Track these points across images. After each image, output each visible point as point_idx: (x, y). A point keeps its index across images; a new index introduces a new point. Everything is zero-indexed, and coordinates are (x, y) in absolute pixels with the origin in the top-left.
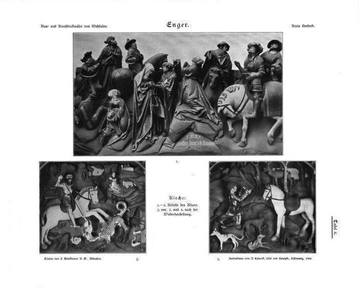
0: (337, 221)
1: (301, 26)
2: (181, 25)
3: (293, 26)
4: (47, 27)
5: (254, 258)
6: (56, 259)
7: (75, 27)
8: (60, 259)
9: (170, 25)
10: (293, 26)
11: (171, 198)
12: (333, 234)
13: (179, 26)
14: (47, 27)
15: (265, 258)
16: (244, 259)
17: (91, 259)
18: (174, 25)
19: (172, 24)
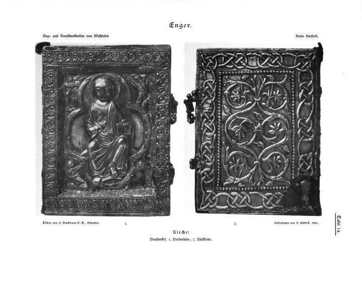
0: (340, 217)
1: (305, 36)
3: (275, 223)
4: (49, 36)
5: (62, 222)
6: (57, 36)
7: (77, 36)
8: (58, 223)
11: (174, 232)
12: (337, 232)
13: (181, 27)
14: (49, 36)
15: (311, 222)
16: (85, 36)
17: (88, 223)
18: (177, 25)
19: (174, 24)
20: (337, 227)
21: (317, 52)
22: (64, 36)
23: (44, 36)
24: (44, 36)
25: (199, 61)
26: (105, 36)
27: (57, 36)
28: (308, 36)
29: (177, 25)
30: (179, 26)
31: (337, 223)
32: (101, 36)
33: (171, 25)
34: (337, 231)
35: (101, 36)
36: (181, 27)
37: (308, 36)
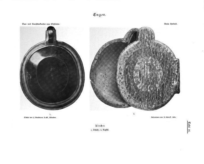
0: (190, 123)
1: (170, 24)
2: (101, 15)
3: (152, 117)
4: (25, 24)
6: (30, 24)
9: (95, 15)
10: (176, 24)
11: (96, 126)
12: (188, 131)
13: (100, 16)
14: (25, 24)
16: (46, 24)
18: (97, 15)
20: (189, 128)
21: (134, 33)
22: (34, 24)
23: (23, 24)
24: (23, 24)
25: (21, 30)
26: (57, 24)
27: (30, 24)
28: (171, 24)
29: (97, 15)
30: (99, 15)
31: (188, 127)
32: (37, 24)
33: (94, 15)
34: (188, 131)
35: (37, 24)
36: (100, 16)
37: (171, 24)
